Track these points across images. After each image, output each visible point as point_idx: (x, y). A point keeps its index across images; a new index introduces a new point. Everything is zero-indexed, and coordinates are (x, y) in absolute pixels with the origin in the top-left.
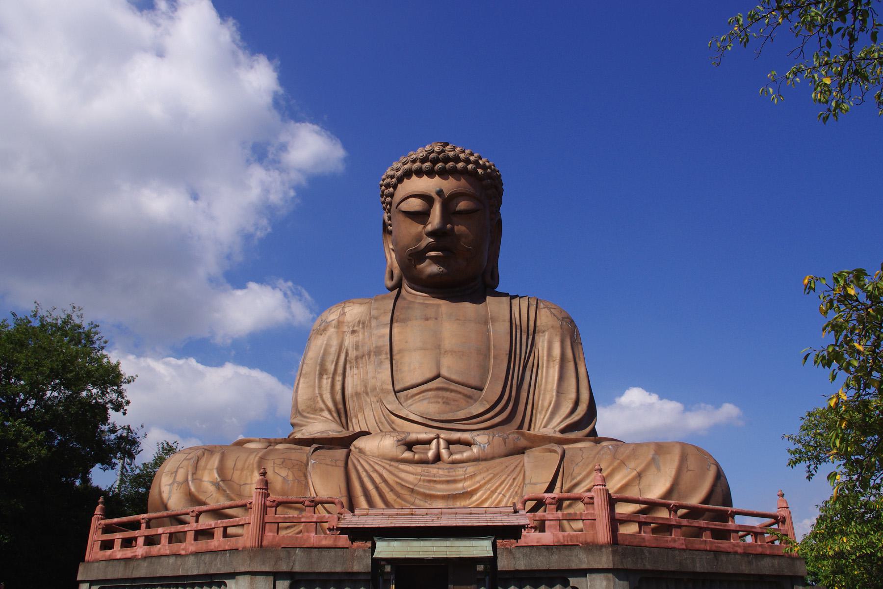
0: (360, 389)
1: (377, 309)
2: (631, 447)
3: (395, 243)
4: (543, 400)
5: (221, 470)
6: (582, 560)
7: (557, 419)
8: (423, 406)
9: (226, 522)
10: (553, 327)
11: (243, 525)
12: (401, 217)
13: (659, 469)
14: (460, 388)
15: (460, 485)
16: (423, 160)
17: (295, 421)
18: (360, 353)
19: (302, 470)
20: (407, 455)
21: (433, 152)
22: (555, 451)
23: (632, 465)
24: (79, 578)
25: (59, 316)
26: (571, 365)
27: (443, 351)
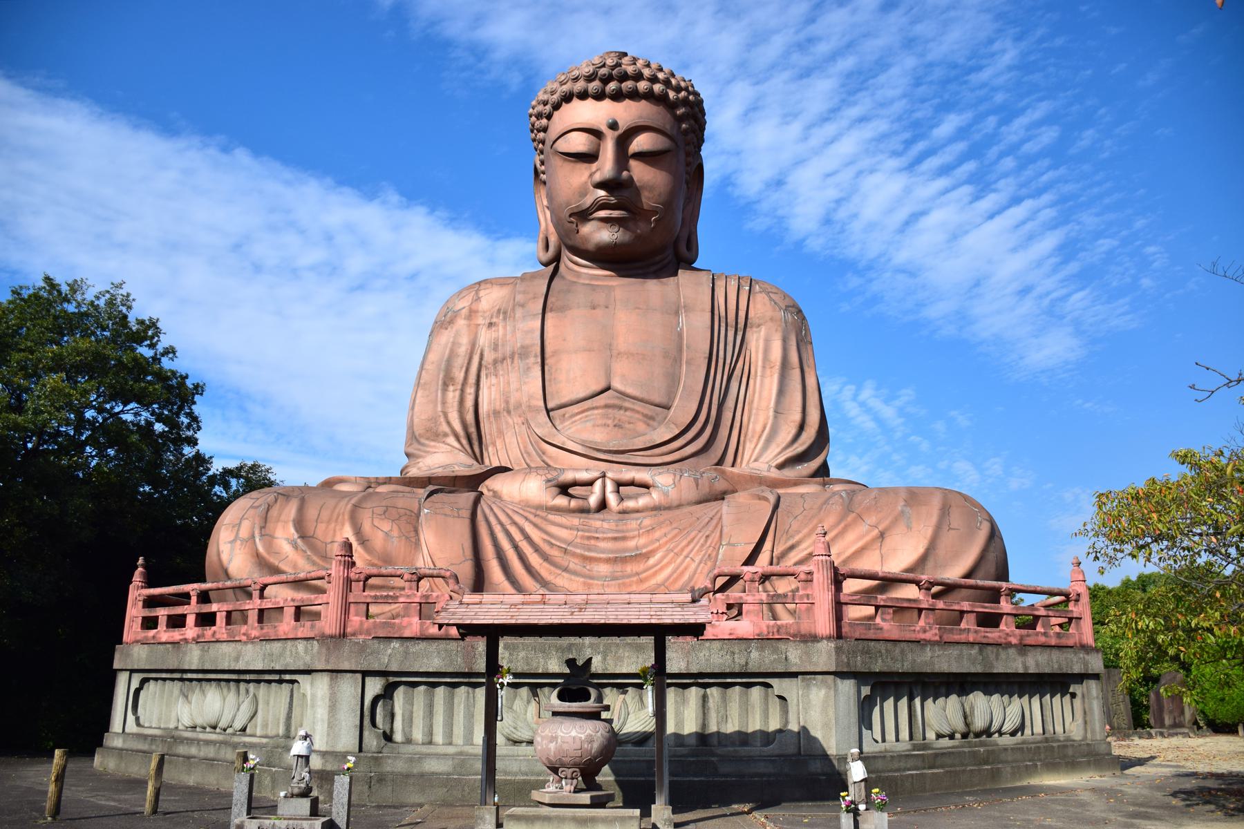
0: (500, 405)
1: (524, 292)
2: (873, 494)
3: (550, 198)
4: (755, 423)
5: (299, 524)
6: (795, 657)
7: (774, 450)
8: (586, 429)
10: (772, 319)
12: (557, 162)
13: (909, 528)
14: (638, 406)
15: (632, 544)
16: (590, 78)
17: (410, 450)
18: (500, 355)
19: (412, 523)
20: (562, 501)
21: (604, 66)
22: (766, 499)
23: (872, 519)
24: (116, 666)
25: (94, 290)
26: (796, 373)
27: (615, 352)
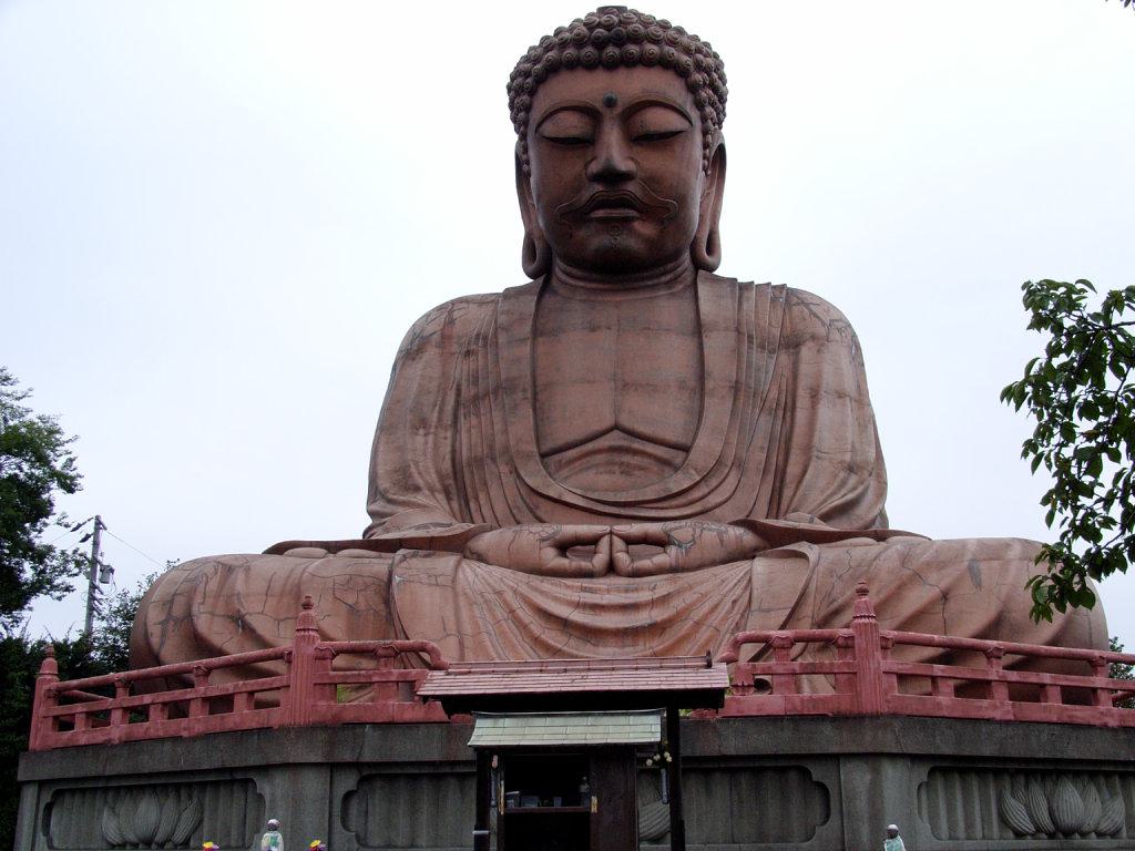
9: (253, 684)
11: (278, 688)
24: (21, 777)
